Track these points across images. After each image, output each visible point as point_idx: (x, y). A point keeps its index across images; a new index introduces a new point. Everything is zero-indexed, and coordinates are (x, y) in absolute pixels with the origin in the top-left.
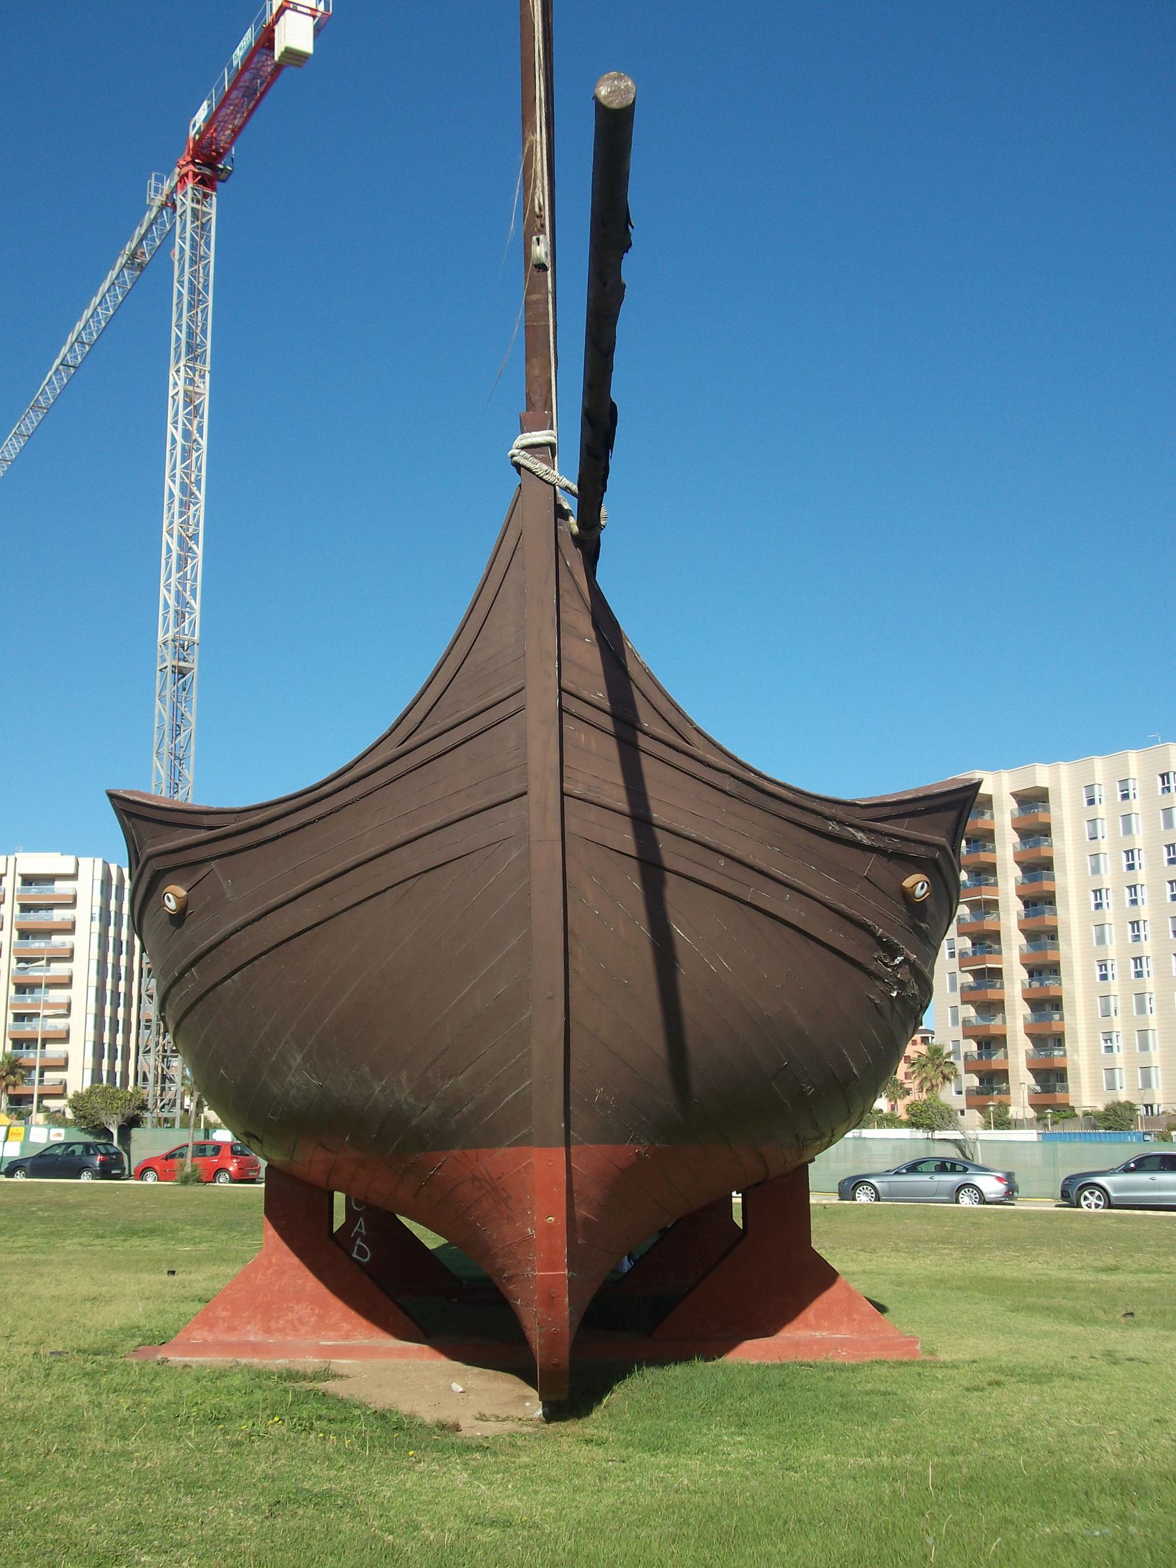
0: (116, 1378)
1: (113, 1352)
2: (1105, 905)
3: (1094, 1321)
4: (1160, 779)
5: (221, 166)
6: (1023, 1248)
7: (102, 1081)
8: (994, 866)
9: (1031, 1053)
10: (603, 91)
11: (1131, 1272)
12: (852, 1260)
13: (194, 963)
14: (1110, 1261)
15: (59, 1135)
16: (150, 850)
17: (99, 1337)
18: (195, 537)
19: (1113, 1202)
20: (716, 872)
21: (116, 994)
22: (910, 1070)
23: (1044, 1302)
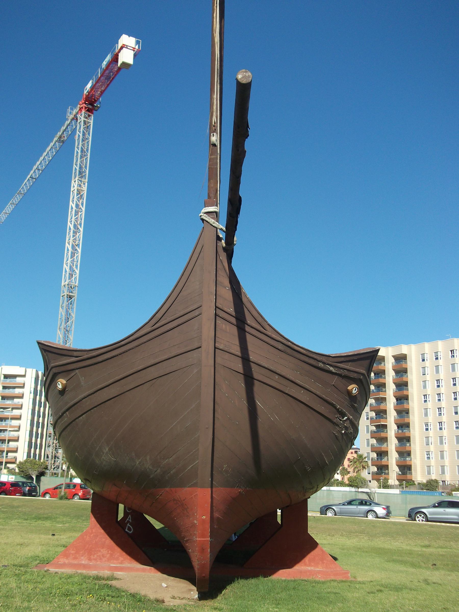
0: (28, 577)
1: (27, 566)
2: (428, 401)
3: (420, 567)
4: (450, 352)
5: (95, 105)
6: (393, 537)
7: (30, 457)
8: (385, 384)
9: (398, 459)
10: (240, 77)
11: (435, 548)
12: (324, 539)
13: (68, 410)
14: (427, 543)
15: (12, 478)
16: (52, 365)
17: (22, 560)
18: (78, 245)
19: (429, 519)
20: (274, 381)
21: (38, 423)
22: (350, 464)
23: (400, 558)
